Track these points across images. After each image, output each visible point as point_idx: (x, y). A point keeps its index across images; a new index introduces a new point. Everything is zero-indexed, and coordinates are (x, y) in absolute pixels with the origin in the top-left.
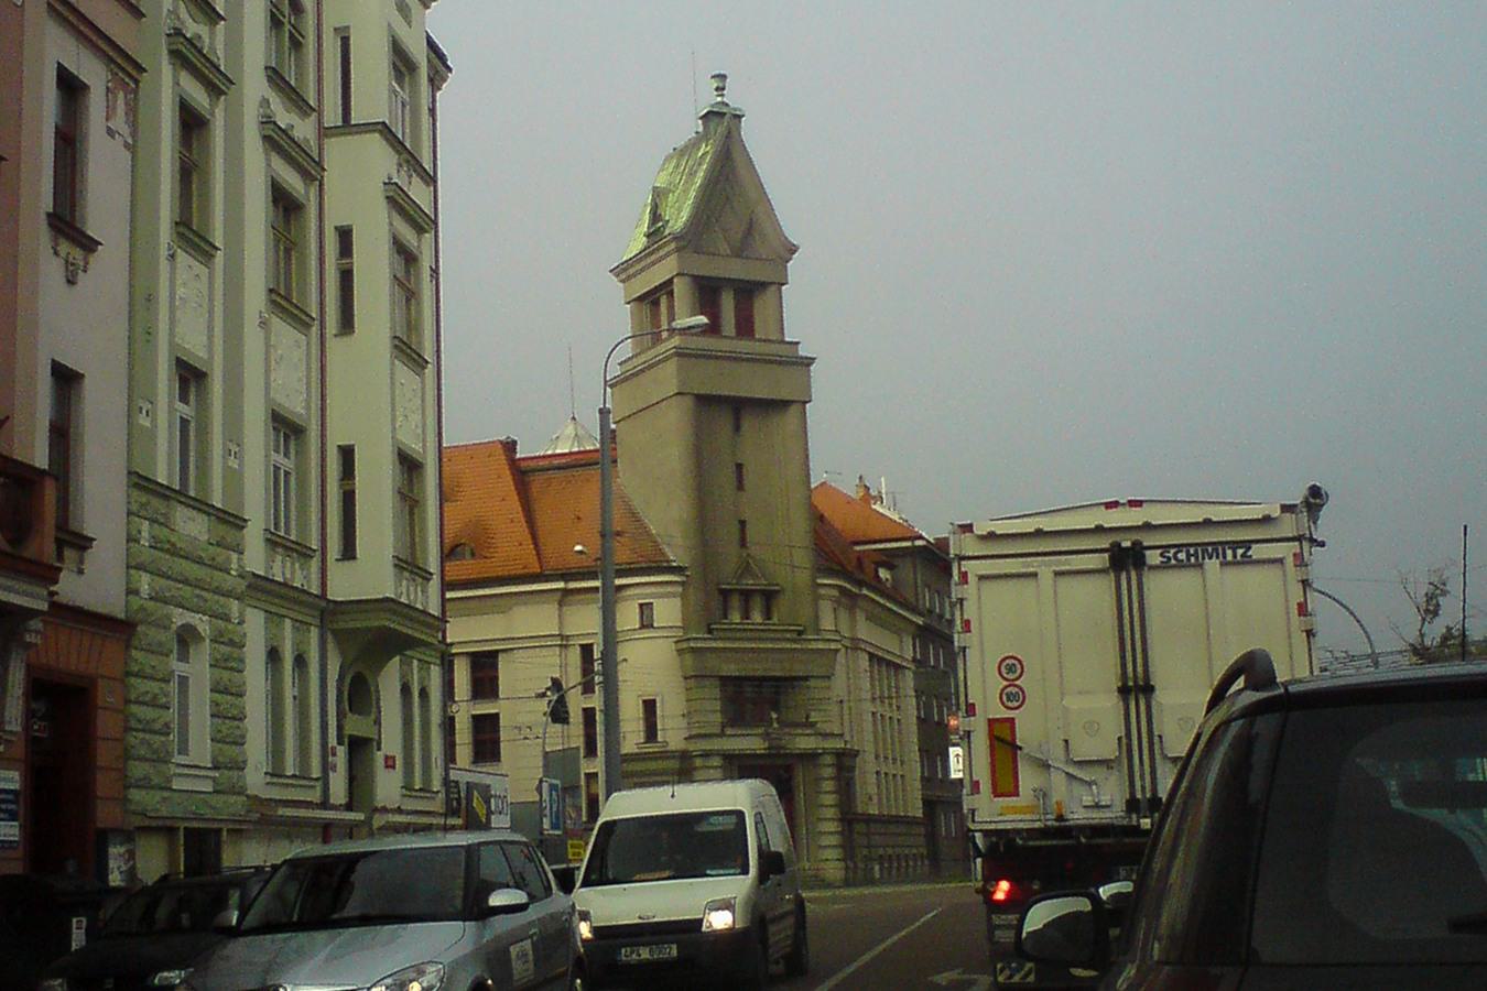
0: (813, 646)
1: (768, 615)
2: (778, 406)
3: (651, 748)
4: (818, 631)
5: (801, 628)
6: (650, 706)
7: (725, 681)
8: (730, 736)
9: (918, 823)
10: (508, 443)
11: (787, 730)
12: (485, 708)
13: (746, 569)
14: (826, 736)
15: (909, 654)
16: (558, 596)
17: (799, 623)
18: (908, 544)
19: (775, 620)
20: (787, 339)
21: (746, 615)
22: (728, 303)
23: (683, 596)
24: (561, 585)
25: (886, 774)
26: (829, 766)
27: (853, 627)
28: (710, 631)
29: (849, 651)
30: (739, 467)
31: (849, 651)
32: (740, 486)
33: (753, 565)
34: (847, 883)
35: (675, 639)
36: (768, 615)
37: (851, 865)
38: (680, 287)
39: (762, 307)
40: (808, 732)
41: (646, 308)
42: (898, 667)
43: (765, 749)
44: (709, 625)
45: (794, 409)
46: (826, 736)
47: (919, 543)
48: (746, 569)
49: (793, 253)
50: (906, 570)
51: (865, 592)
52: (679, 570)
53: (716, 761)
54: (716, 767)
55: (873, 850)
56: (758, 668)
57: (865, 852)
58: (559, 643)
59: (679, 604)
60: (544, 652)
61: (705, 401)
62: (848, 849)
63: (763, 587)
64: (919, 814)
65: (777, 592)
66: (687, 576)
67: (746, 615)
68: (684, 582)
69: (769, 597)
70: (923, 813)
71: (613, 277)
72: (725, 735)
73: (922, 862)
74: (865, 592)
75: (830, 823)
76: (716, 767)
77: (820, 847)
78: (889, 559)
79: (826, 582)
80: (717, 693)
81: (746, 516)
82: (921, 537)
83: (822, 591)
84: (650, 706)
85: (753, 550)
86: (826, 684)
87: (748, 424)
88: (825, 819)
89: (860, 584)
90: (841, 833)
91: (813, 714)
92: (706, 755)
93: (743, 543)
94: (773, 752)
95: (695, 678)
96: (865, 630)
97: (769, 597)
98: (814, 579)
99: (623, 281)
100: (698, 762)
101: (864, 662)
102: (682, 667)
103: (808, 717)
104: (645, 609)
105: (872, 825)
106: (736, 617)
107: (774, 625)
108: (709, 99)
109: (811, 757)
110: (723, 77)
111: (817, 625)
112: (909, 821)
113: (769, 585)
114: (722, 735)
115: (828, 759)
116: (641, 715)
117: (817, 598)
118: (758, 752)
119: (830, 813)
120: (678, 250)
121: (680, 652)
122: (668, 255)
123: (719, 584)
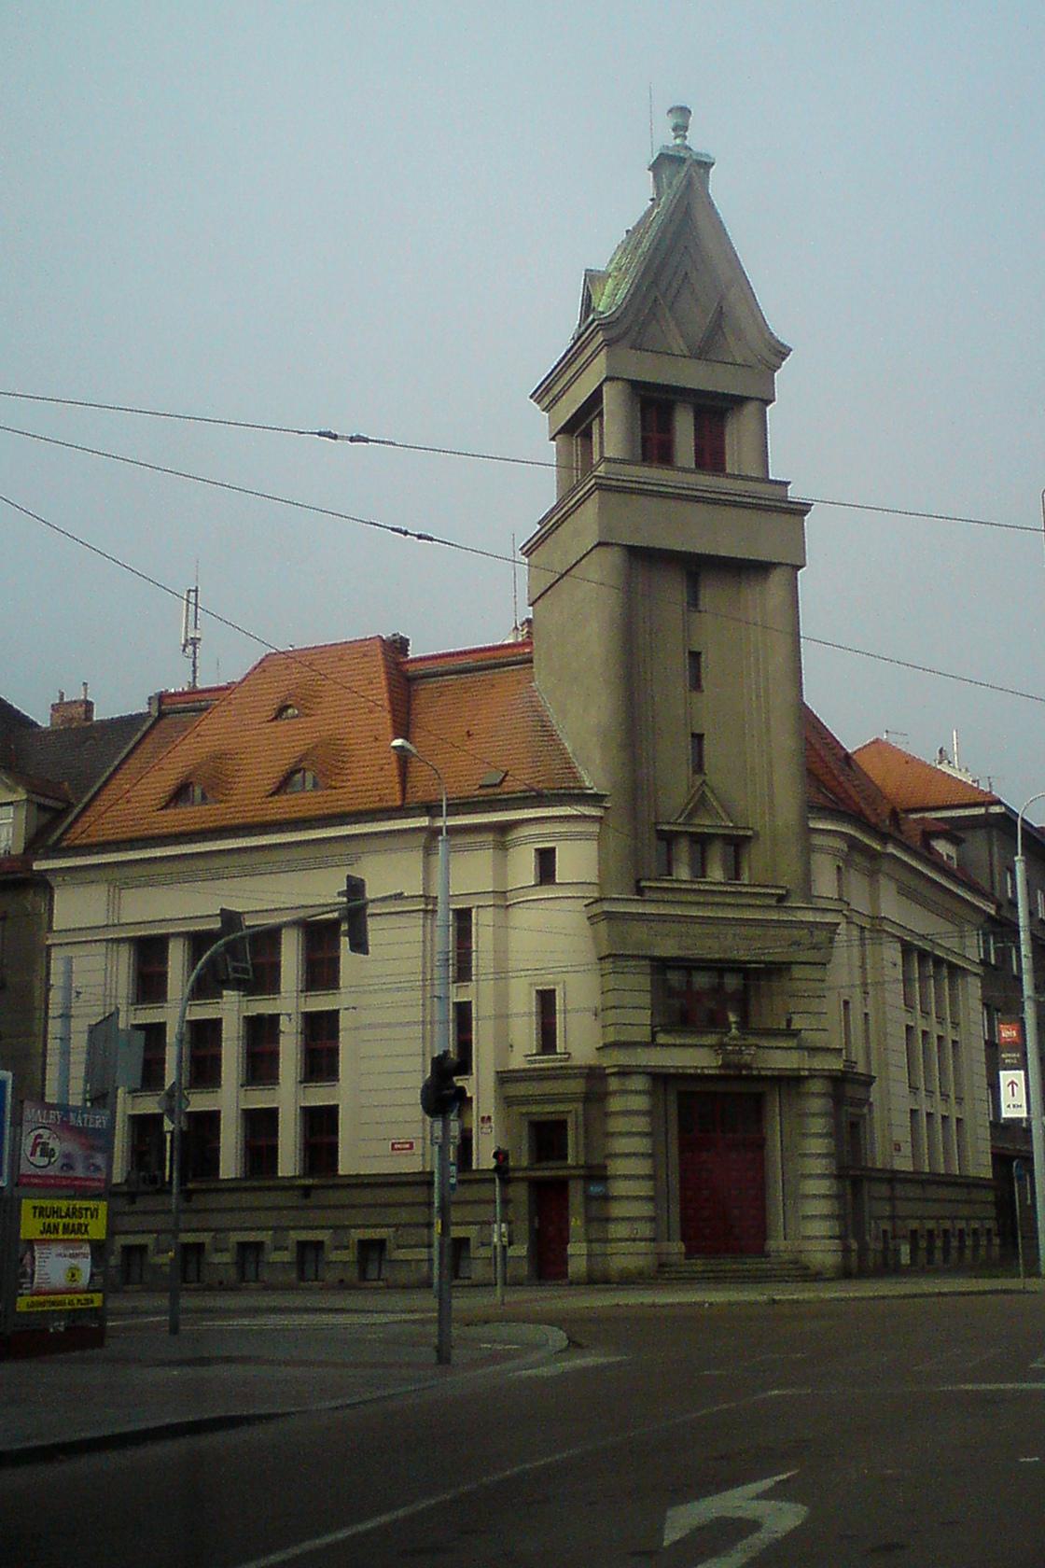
0: (800, 916)
1: (736, 873)
2: (760, 569)
3: (547, 1062)
4: (807, 894)
5: (780, 892)
6: (546, 1000)
7: (661, 965)
8: (662, 1045)
9: (985, 1187)
10: (395, 641)
11: (752, 1040)
12: (320, 1003)
13: (699, 803)
14: (814, 1050)
15: (975, 954)
16: (422, 838)
17: (781, 884)
18: (983, 811)
19: (745, 879)
20: (771, 477)
21: (700, 870)
22: (684, 427)
23: (600, 838)
24: (424, 822)
25: (929, 1115)
26: (517, 1015)
27: (874, 899)
28: (640, 891)
29: (867, 934)
30: (695, 656)
31: (867, 934)
32: (696, 685)
33: (709, 795)
34: (845, 1273)
35: (587, 902)
36: (736, 873)
37: (855, 1246)
38: (613, 401)
39: (737, 435)
40: (790, 1044)
41: (577, 443)
42: (955, 970)
43: (719, 1067)
44: (638, 881)
45: (777, 577)
46: (814, 1050)
47: (996, 809)
48: (699, 803)
49: (783, 359)
50: (978, 845)
51: (891, 849)
52: (596, 799)
53: (639, 1083)
54: (637, 1092)
55: (899, 1223)
56: (709, 948)
57: (886, 1225)
58: (422, 907)
59: (595, 854)
60: (402, 921)
61: (642, 558)
62: (850, 1218)
63: (726, 832)
64: (987, 1173)
65: (749, 838)
66: (606, 808)
67: (700, 870)
68: (601, 818)
69: (737, 844)
70: (994, 1173)
71: (535, 404)
72: (657, 1045)
73: (990, 1240)
74: (891, 849)
75: (818, 1182)
76: (637, 1092)
77: (805, 1217)
78: (953, 831)
79: (821, 826)
80: (645, 982)
81: (705, 726)
82: (999, 803)
83: (818, 840)
84: (546, 1000)
85: (714, 776)
86: (817, 975)
87: (708, 596)
88: (810, 1176)
89: (884, 838)
90: (838, 1197)
91: (795, 1017)
92: (624, 1072)
93: (699, 767)
94: (731, 1072)
95: (612, 959)
96: (892, 907)
97: (737, 844)
98: (805, 820)
99: (546, 409)
100: (614, 1084)
101: (893, 953)
102: (595, 938)
103: (789, 1022)
104: (546, 860)
105: (898, 1186)
106: (683, 872)
107: (745, 885)
108: (668, 139)
109: (791, 1082)
110: (684, 111)
111: (810, 889)
112: (978, 1184)
113: (736, 827)
114: (652, 1043)
115: (817, 1086)
116: (534, 1010)
117: (808, 850)
118: (706, 1072)
119: (818, 1166)
120: (608, 343)
121: (592, 919)
122: (595, 355)
123: (657, 823)
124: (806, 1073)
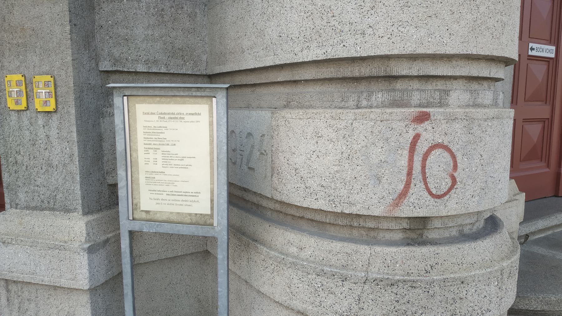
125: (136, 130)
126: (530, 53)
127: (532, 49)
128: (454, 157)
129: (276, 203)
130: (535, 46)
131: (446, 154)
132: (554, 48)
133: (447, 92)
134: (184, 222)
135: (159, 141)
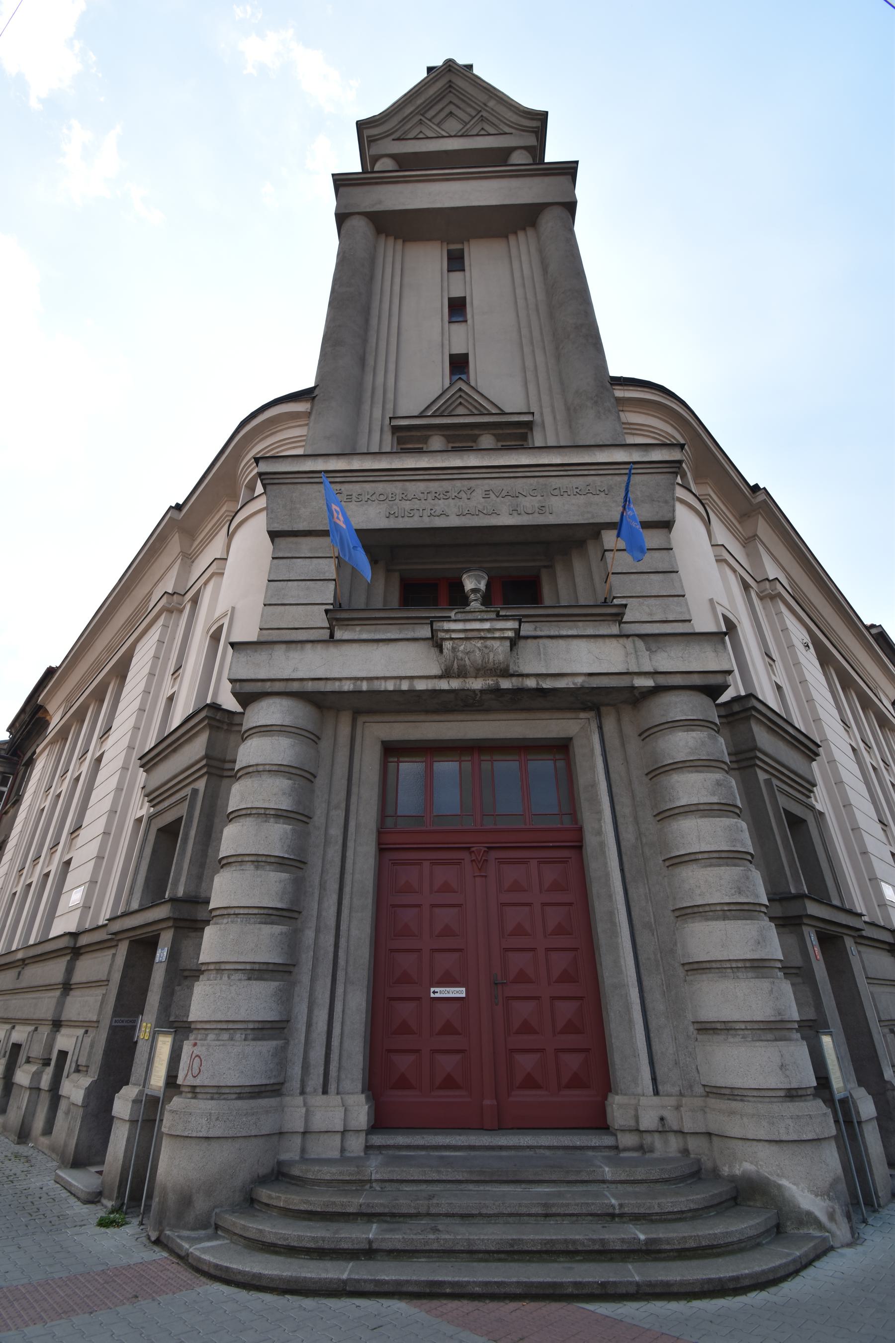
124: (649, 683)
125: (255, 1276)
126: (432, 995)
127: (434, 992)
128: (201, 1061)
129: (361, 1207)
130: (437, 989)
131: (199, 1059)
132: (464, 989)
133: (207, 1035)
134: (592, 640)
135: (350, 921)
